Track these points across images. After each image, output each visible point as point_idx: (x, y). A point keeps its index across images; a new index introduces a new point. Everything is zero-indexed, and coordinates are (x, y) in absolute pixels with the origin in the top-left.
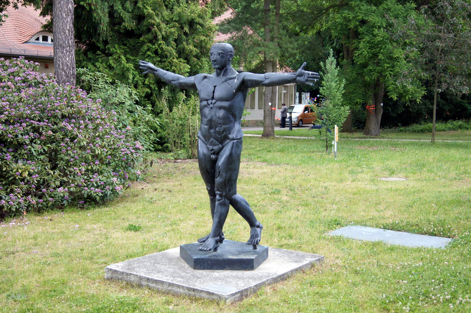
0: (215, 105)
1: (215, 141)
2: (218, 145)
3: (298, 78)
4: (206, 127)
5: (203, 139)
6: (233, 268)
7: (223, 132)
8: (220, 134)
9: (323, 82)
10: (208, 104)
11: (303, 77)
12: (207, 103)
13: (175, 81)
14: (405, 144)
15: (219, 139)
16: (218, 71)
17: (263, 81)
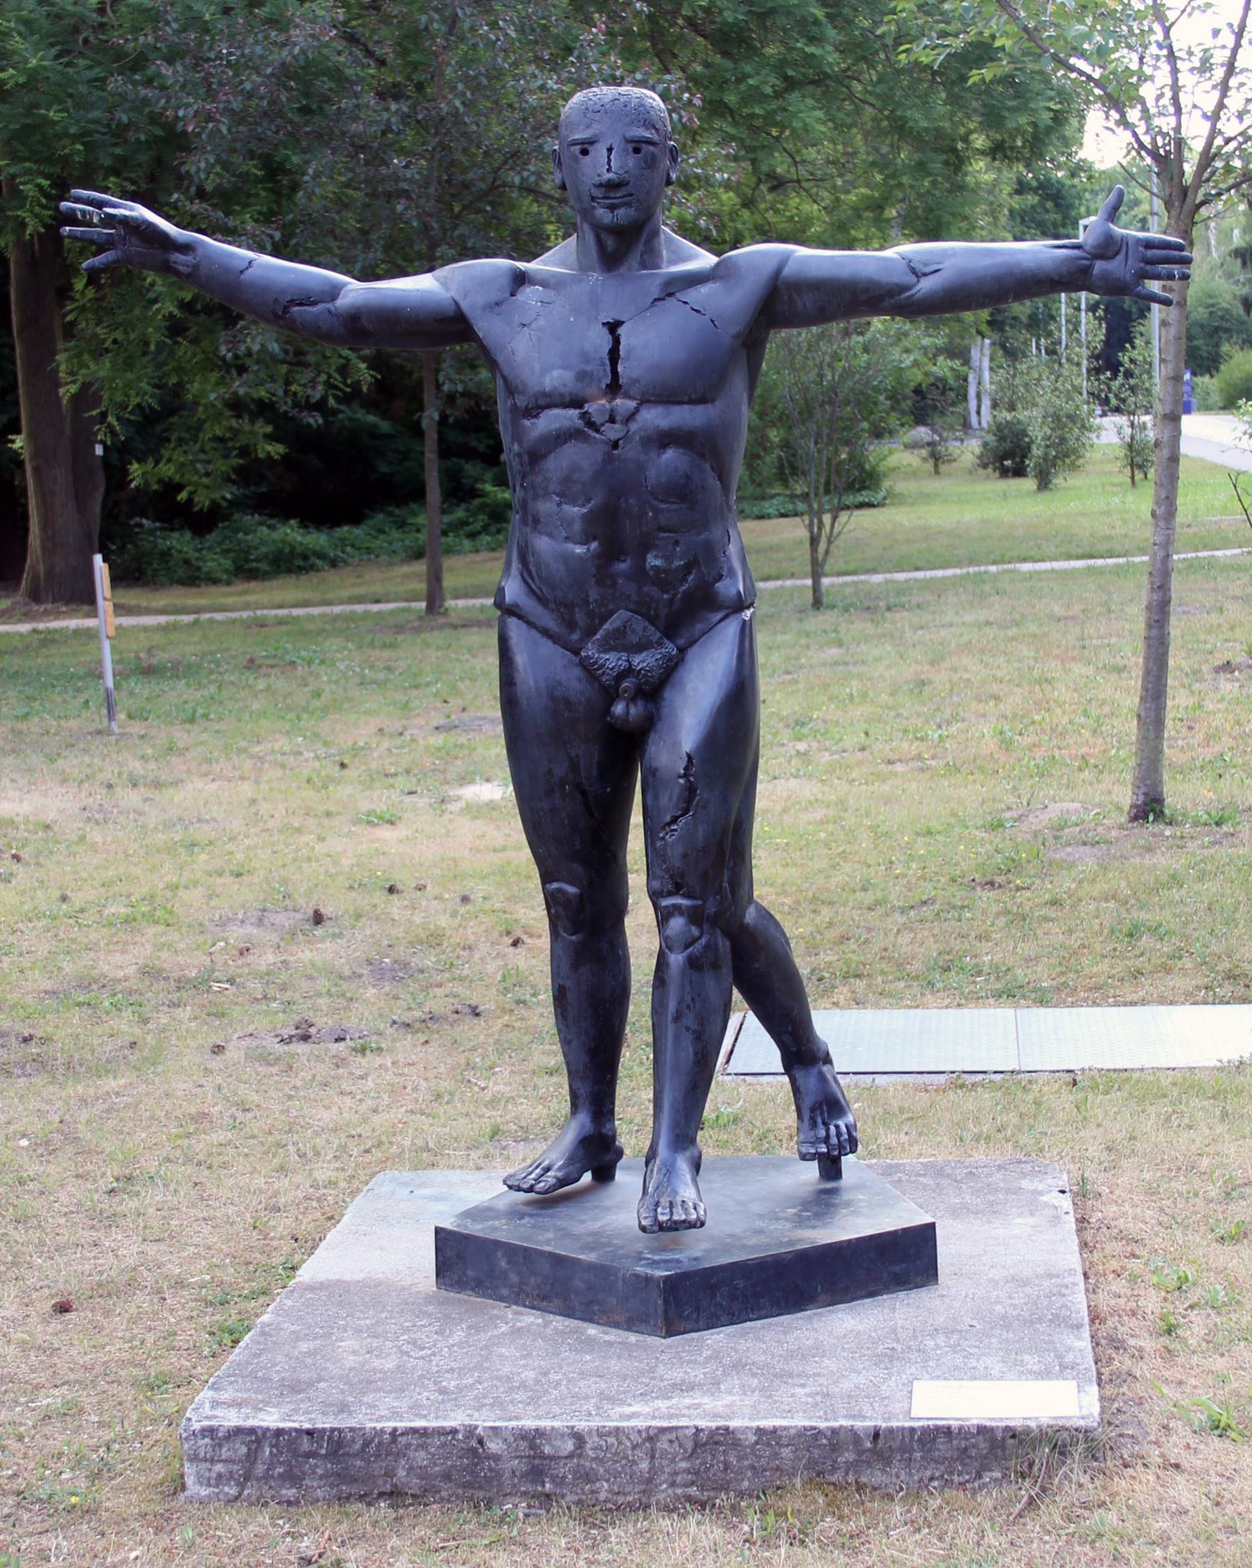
0: (633, 427)
1: (639, 624)
2: (660, 644)
3: (1099, 266)
4: (579, 550)
5: (547, 619)
6: (846, 1290)
7: (688, 568)
8: (664, 586)
9: (269, 429)
10: (591, 424)
11: (1121, 257)
12: (585, 416)
13: (314, 303)
14: (303, 632)
15: (664, 611)
16: (610, 242)
17: (908, 288)
